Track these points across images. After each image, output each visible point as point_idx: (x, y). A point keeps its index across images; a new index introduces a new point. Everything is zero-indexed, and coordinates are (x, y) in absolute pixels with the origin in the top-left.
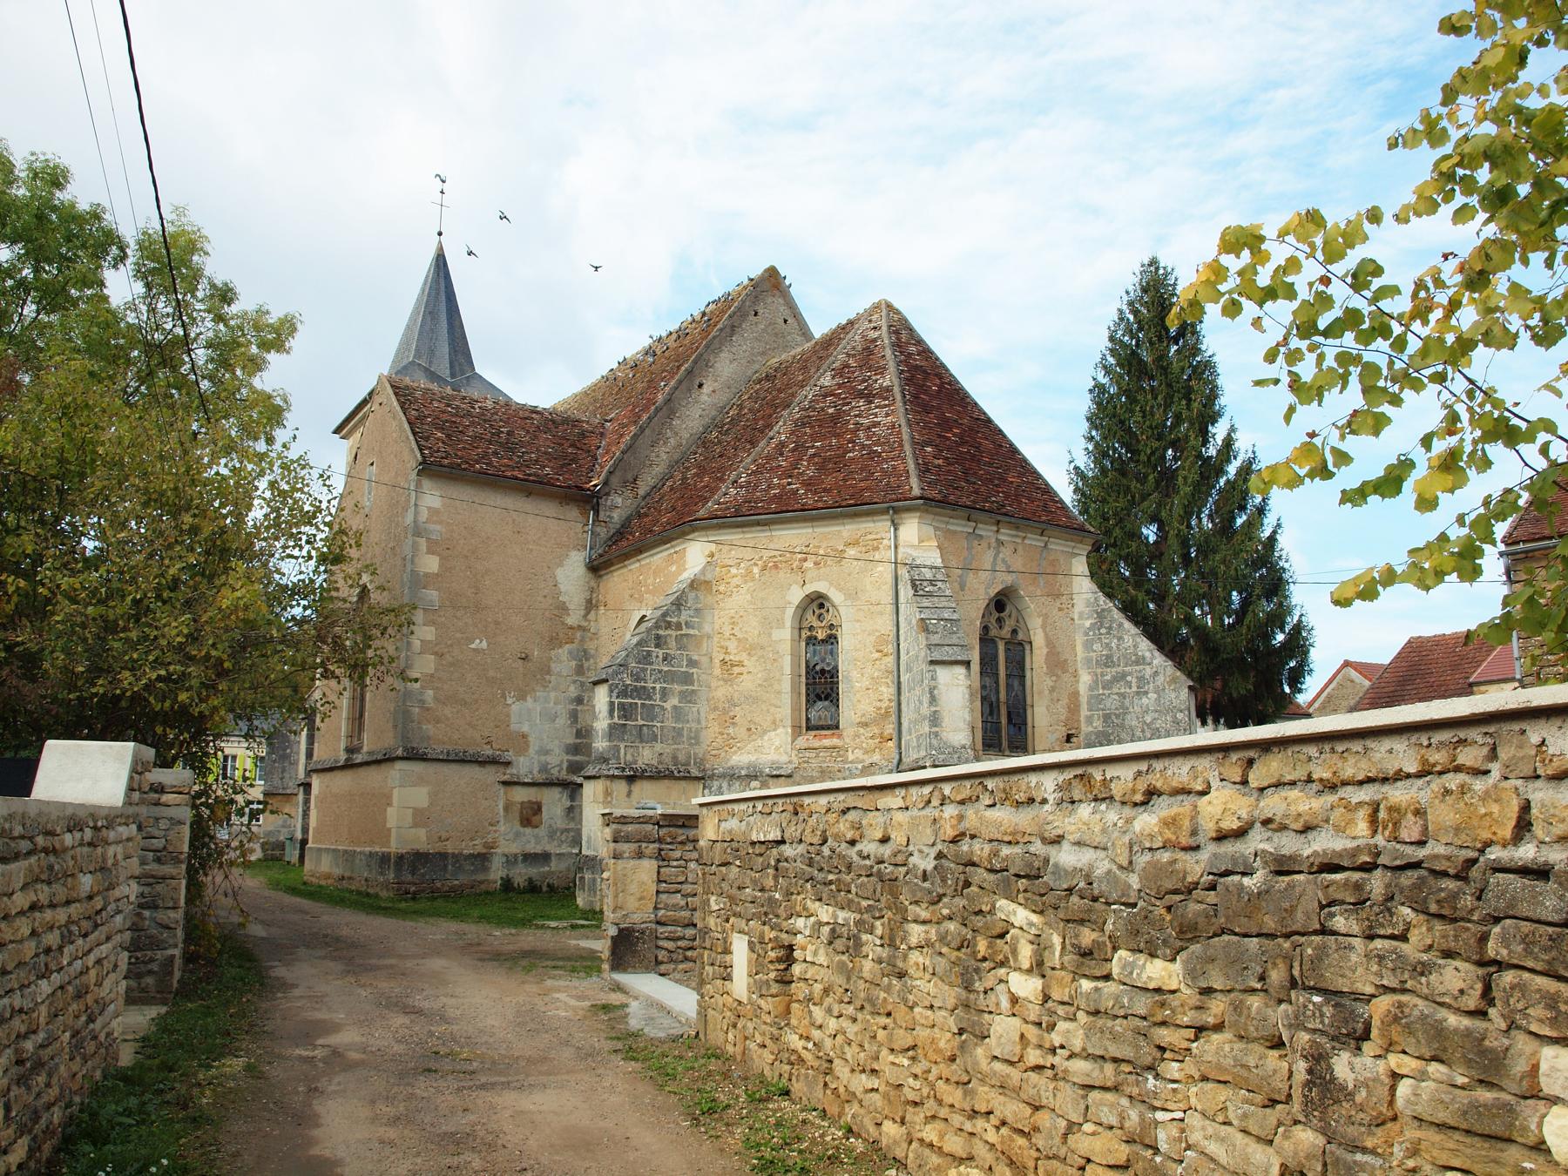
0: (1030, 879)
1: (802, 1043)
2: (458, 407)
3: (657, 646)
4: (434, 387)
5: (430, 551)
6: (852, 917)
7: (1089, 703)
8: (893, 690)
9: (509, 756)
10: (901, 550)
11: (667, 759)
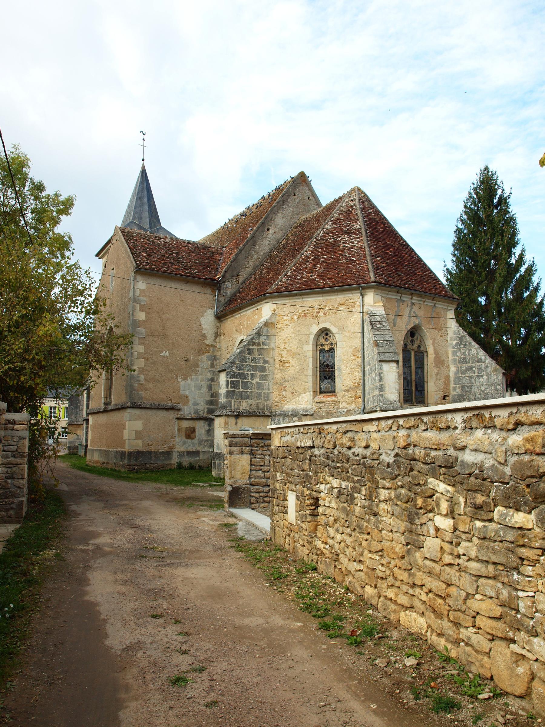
0: (448, 469)
1: (323, 545)
2: (153, 241)
3: (249, 354)
4: (142, 232)
5: (141, 310)
6: (350, 485)
7: (454, 381)
8: (361, 374)
9: (180, 406)
10: (365, 307)
11: (254, 407)
